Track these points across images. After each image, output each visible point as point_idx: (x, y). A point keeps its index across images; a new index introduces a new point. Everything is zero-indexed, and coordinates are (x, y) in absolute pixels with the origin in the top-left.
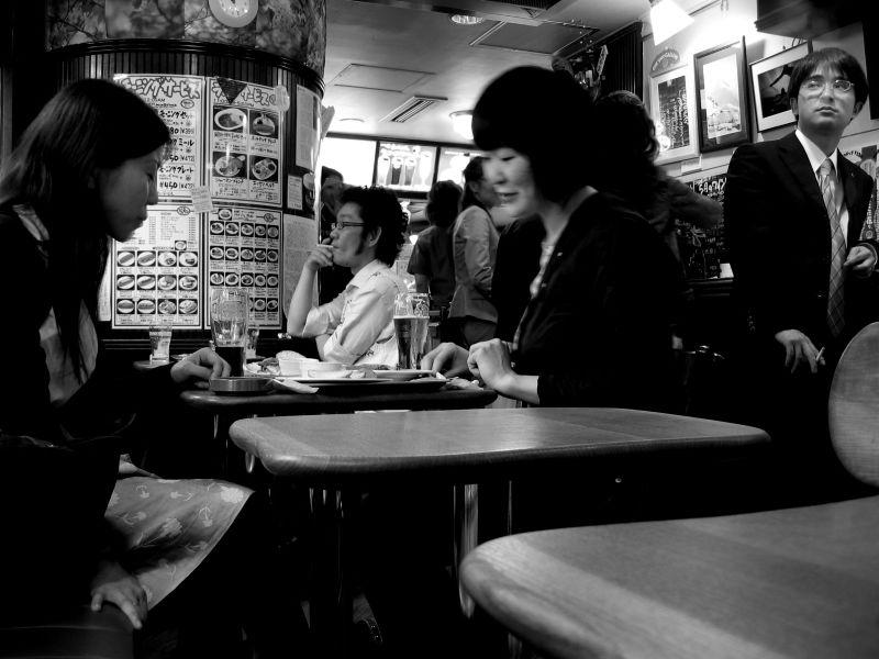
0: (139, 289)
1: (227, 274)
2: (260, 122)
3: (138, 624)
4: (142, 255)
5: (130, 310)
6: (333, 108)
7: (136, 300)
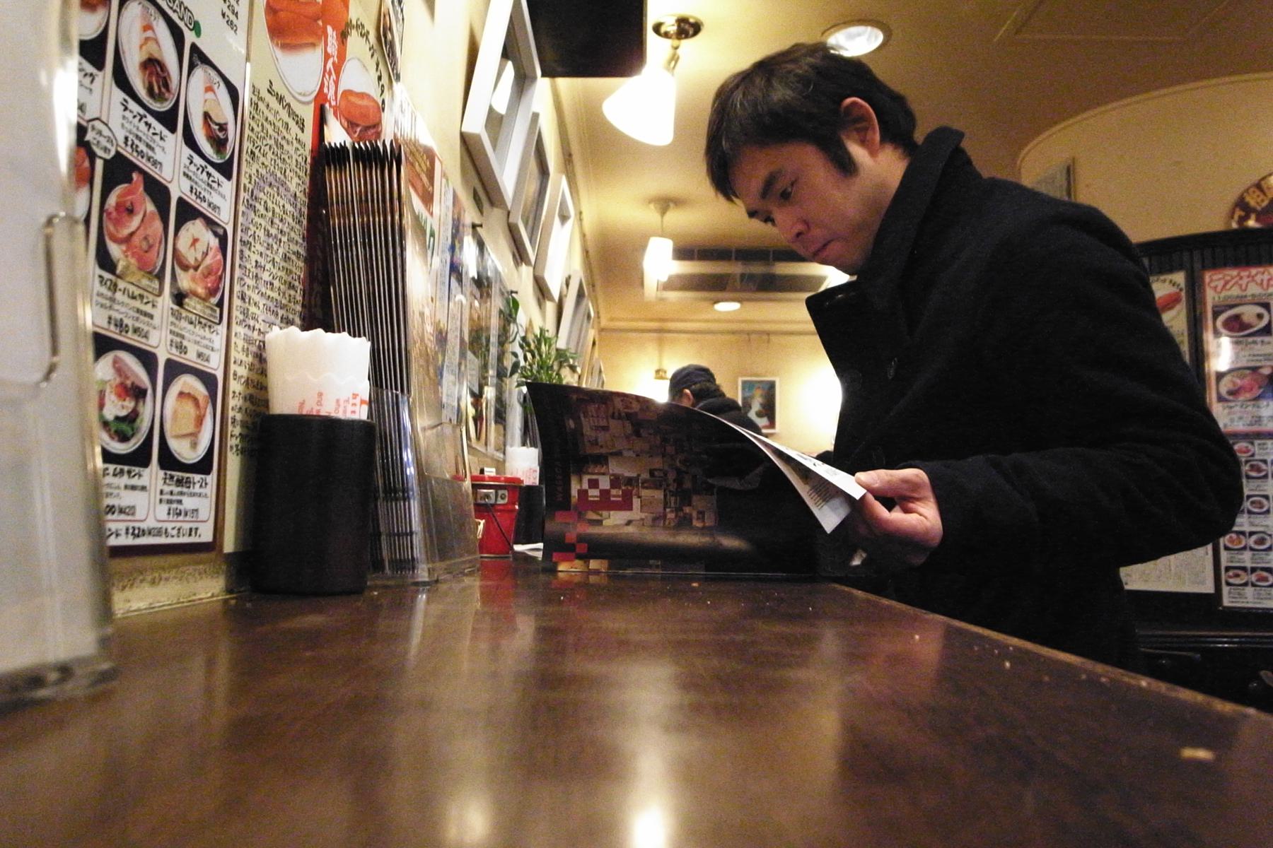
1: (1252, 534)
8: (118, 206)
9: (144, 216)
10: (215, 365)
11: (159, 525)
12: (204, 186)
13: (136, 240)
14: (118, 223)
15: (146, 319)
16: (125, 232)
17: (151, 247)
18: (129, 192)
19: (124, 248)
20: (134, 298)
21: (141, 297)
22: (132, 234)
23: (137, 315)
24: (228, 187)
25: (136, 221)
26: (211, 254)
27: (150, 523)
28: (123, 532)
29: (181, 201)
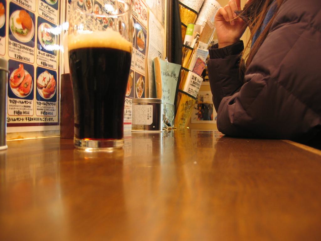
8: (15, 77)
9: (25, 76)
10: (55, 68)
11: (38, 117)
12: (47, 12)
13: (22, 85)
14: (15, 82)
15: (28, 108)
16: (18, 84)
17: (27, 86)
18: (19, 71)
19: (18, 89)
20: (23, 103)
21: (25, 102)
22: (20, 84)
23: (24, 108)
24: (56, 12)
25: (22, 79)
26: (51, 81)
27: (35, 116)
28: (25, 119)
29: (39, 17)
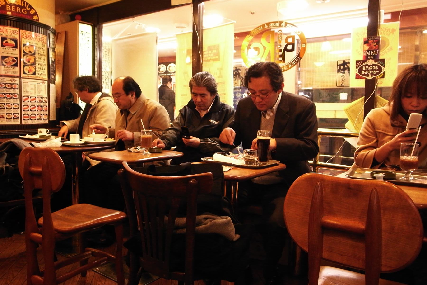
0: (31, 110)
2: (7, 42)
3: (374, 175)
4: (32, 98)
5: (28, 119)
6: (356, 78)
7: (30, 115)
